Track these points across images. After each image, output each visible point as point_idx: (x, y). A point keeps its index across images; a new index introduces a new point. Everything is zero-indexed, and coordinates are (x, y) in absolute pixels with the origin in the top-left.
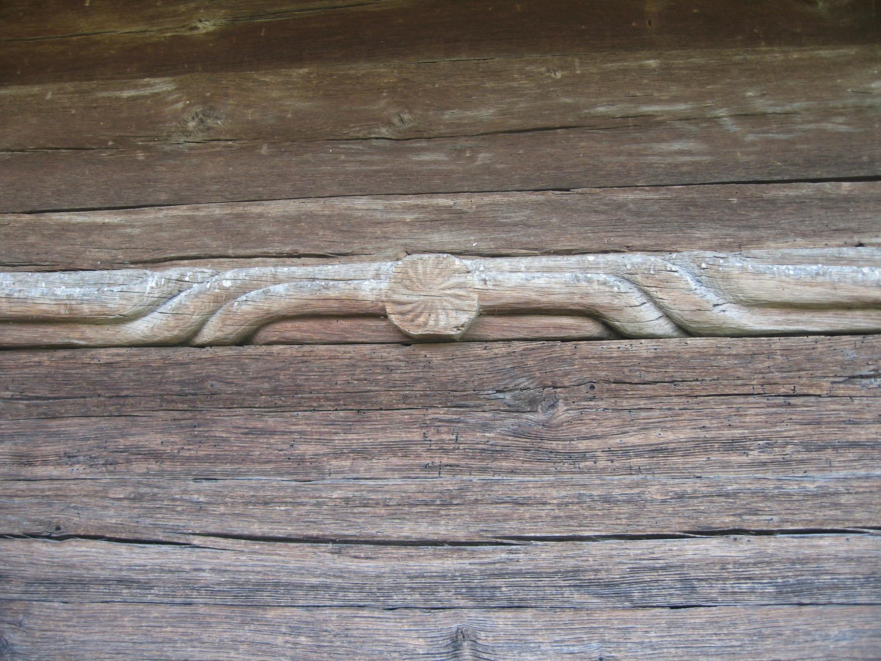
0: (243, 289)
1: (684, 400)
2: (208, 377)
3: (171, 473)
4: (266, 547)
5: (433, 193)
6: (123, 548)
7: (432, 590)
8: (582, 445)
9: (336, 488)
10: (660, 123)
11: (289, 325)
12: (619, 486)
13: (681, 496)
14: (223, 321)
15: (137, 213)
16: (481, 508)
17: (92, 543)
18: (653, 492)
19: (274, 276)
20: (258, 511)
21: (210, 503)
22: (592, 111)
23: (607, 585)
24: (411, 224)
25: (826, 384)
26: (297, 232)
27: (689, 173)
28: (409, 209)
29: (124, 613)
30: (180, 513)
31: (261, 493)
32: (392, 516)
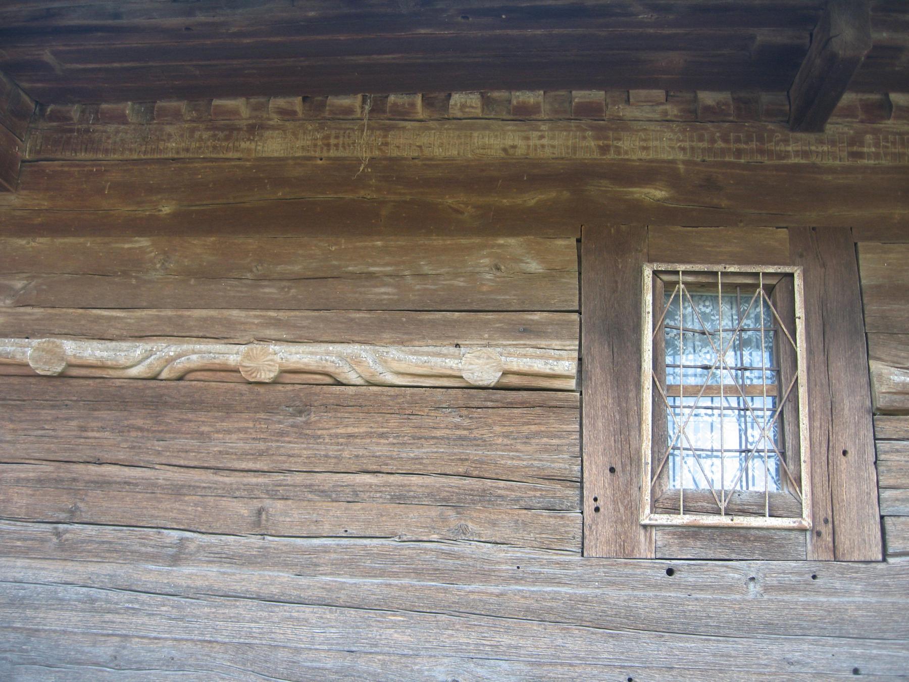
0: (179, 356)
1: (364, 414)
2: (164, 395)
3: (147, 437)
4: (186, 470)
5: (268, 309)
6: (126, 469)
7: (252, 490)
8: (319, 432)
9: (216, 446)
10: (377, 277)
11: (199, 373)
12: (332, 451)
13: (357, 456)
14: (170, 371)
15: (133, 312)
16: (274, 457)
17: (113, 466)
18: (346, 454)
19: (193, 350)
20: (183, 455)
21: (163, 451)
22: (346, 269)
23: (322, 492)
24: (257, 325)
25: (426, 410)
26: (206, 325)
27: (386, 304)
28: (257, 317)
29: (127, 496)
30: (150, 455)
31: (184, 447)
32: (238, 459)
